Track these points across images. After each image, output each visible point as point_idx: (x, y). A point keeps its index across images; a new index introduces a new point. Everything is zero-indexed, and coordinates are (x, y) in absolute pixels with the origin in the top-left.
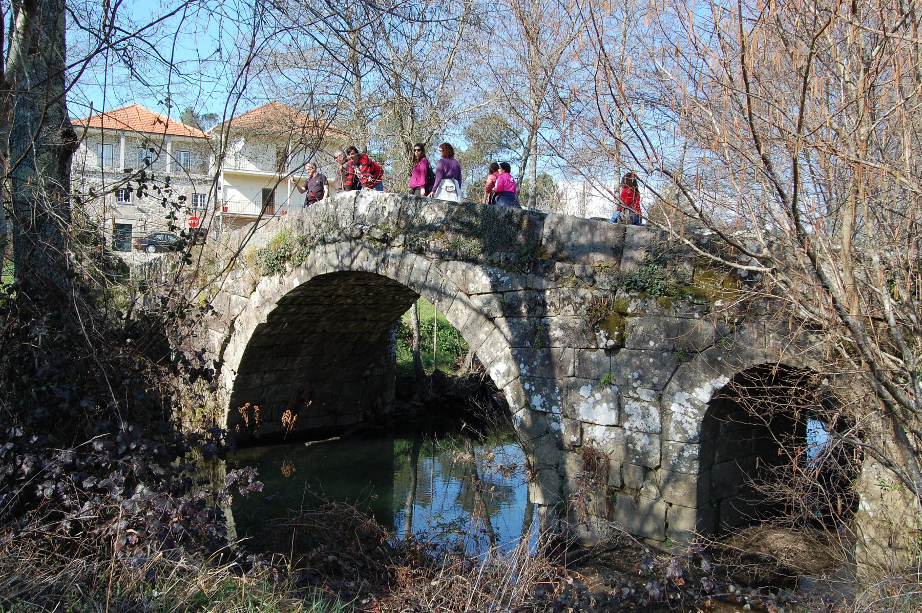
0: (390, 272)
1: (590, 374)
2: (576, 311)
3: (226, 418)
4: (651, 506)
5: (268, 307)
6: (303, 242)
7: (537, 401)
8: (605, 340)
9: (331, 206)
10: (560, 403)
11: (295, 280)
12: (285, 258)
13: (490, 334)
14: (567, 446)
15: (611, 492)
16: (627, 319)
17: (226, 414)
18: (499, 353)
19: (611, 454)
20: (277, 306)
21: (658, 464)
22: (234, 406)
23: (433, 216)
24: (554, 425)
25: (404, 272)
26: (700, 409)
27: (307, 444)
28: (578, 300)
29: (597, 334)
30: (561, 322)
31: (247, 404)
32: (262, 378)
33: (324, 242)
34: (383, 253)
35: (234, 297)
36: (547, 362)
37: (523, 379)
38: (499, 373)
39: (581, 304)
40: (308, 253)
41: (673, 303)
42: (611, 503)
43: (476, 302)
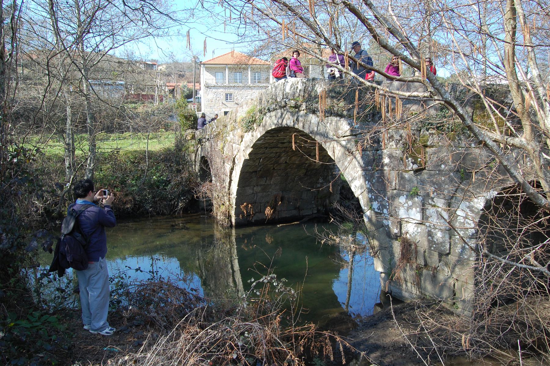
0: (299, 126)
2: (396, 146)
3: (234, 211)
4: (446, 280)
5: (248, 150)
6: (261, 111)
7: (375, 205)
8: (411, 164)
9: (274, 89)
10: (388, 207)
11: (258, 133)
12: (254, 122)
13: (350, 163)
15: (419, 268)
18: (355, 174)
19: (418, 242)
21: (448, 252)
24: (385, 222)
25: (307, 126)
26: (477, 213)
27: (278, 226)
28: (399, 138)
29: (407, 160)
31: (245, 204)
32: (253, 189)
33: (269, 111)
34: (297, 115)
35: (234, 145)
36: (380, 180)
37: (370, 191)
39: (399, 141)
40: (263, 118)
41: (457, 137)
42: (419, 275)
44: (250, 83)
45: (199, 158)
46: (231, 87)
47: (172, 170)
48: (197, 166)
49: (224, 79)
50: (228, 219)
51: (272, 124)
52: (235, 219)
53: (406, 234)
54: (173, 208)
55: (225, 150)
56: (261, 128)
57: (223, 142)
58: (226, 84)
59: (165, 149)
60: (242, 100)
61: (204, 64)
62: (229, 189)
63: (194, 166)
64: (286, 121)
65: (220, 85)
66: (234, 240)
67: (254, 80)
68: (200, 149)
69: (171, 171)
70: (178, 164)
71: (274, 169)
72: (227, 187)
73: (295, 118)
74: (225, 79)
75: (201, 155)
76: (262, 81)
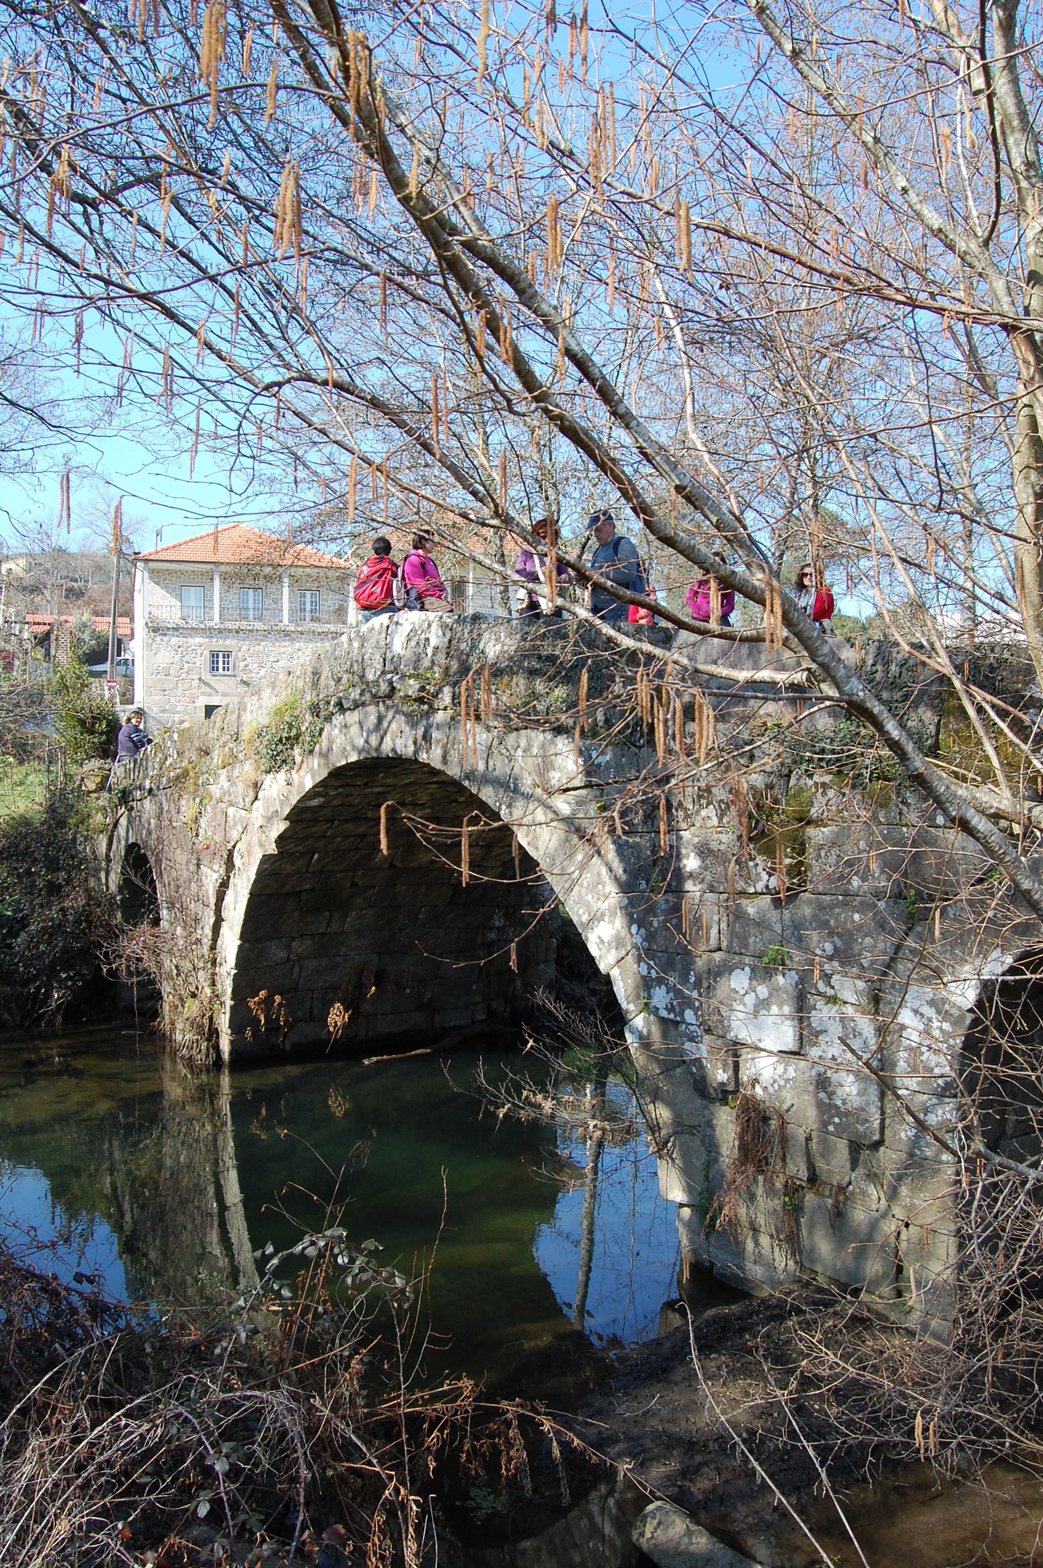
0: (432, 757)
1: (746, 946)
3: (228, 1015)
4: (874, 1225)
5: (275, 827)
8: (764, 876)
9: (356, 644)
10: (697, 1004)
12: (294, 740)
14: (712, 1091)
15: (792, 1190)
16: (811, 831)
17: (228, 1009)
18: (600, 903)
19: (788, 1111)
20: (288, 823)
22: (240, 993)
23: (498, 648)
25: (454, 757)
26: (956, 1022)
30: (696, 840)
32: (289, 948)
34: (424, 722)
35: (231, 811)
38: (602, 941)
40: (322, 730)
42: (794, 1210)
43: (563, 805)
44: (286, 621)
45: (119, 849)
46: (230, 631)
47: (33, 885)
48: (113, 876)
49: (207, 604)
50: (209, 1040)
51: (349, 748)
52: (232, 1043)
53: (754, 1087)
54: (33, 1006)
55: (203, 825)
56: (316, 762)
57: (198, 800)
58: (211, 624)
59: (13, 819)
60: (262, 672)
61: (146, 561)
62: (213, 947)
63: (103, 875)
64: (393, 741)
65: (193, 623)
66: (226, 1109)
67: (298, 612)
68: (123, 821)
69: (31, 890)
70: (53, 866)
71: (354, 885)
72: (207, 942)
73: (421, 731)
74: (211, 608)
75: (127, 840)
76: (324, 616)
